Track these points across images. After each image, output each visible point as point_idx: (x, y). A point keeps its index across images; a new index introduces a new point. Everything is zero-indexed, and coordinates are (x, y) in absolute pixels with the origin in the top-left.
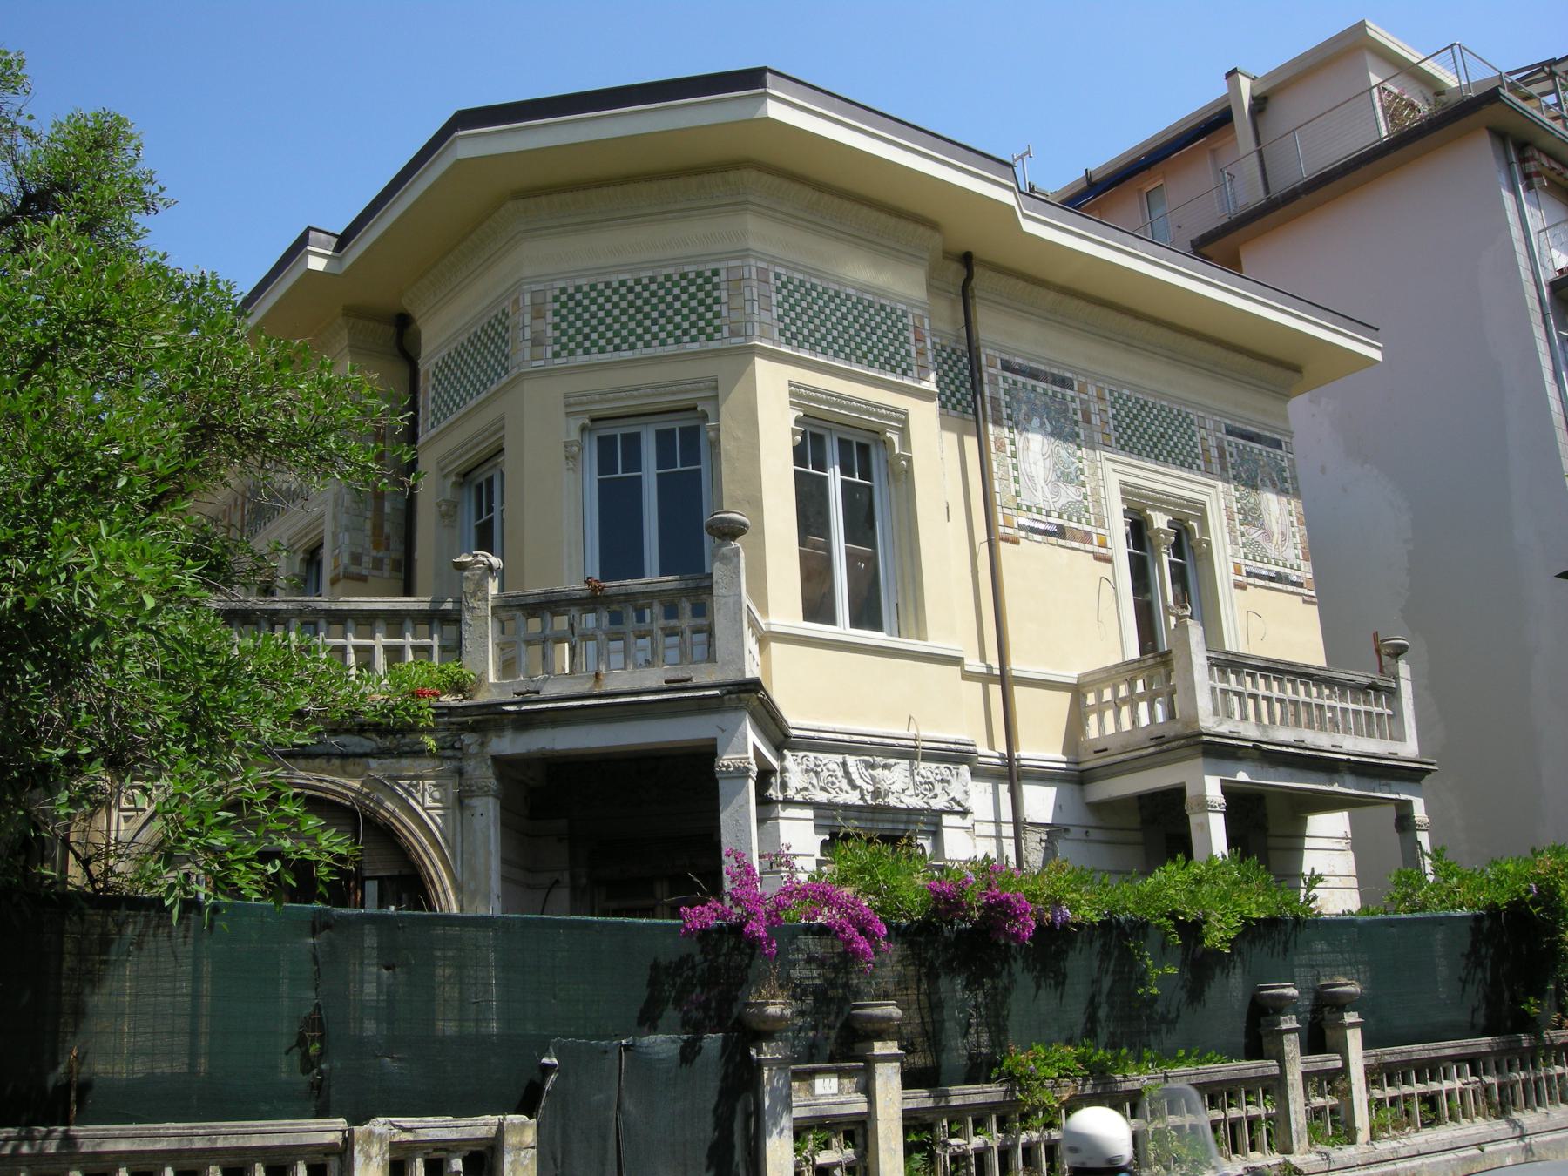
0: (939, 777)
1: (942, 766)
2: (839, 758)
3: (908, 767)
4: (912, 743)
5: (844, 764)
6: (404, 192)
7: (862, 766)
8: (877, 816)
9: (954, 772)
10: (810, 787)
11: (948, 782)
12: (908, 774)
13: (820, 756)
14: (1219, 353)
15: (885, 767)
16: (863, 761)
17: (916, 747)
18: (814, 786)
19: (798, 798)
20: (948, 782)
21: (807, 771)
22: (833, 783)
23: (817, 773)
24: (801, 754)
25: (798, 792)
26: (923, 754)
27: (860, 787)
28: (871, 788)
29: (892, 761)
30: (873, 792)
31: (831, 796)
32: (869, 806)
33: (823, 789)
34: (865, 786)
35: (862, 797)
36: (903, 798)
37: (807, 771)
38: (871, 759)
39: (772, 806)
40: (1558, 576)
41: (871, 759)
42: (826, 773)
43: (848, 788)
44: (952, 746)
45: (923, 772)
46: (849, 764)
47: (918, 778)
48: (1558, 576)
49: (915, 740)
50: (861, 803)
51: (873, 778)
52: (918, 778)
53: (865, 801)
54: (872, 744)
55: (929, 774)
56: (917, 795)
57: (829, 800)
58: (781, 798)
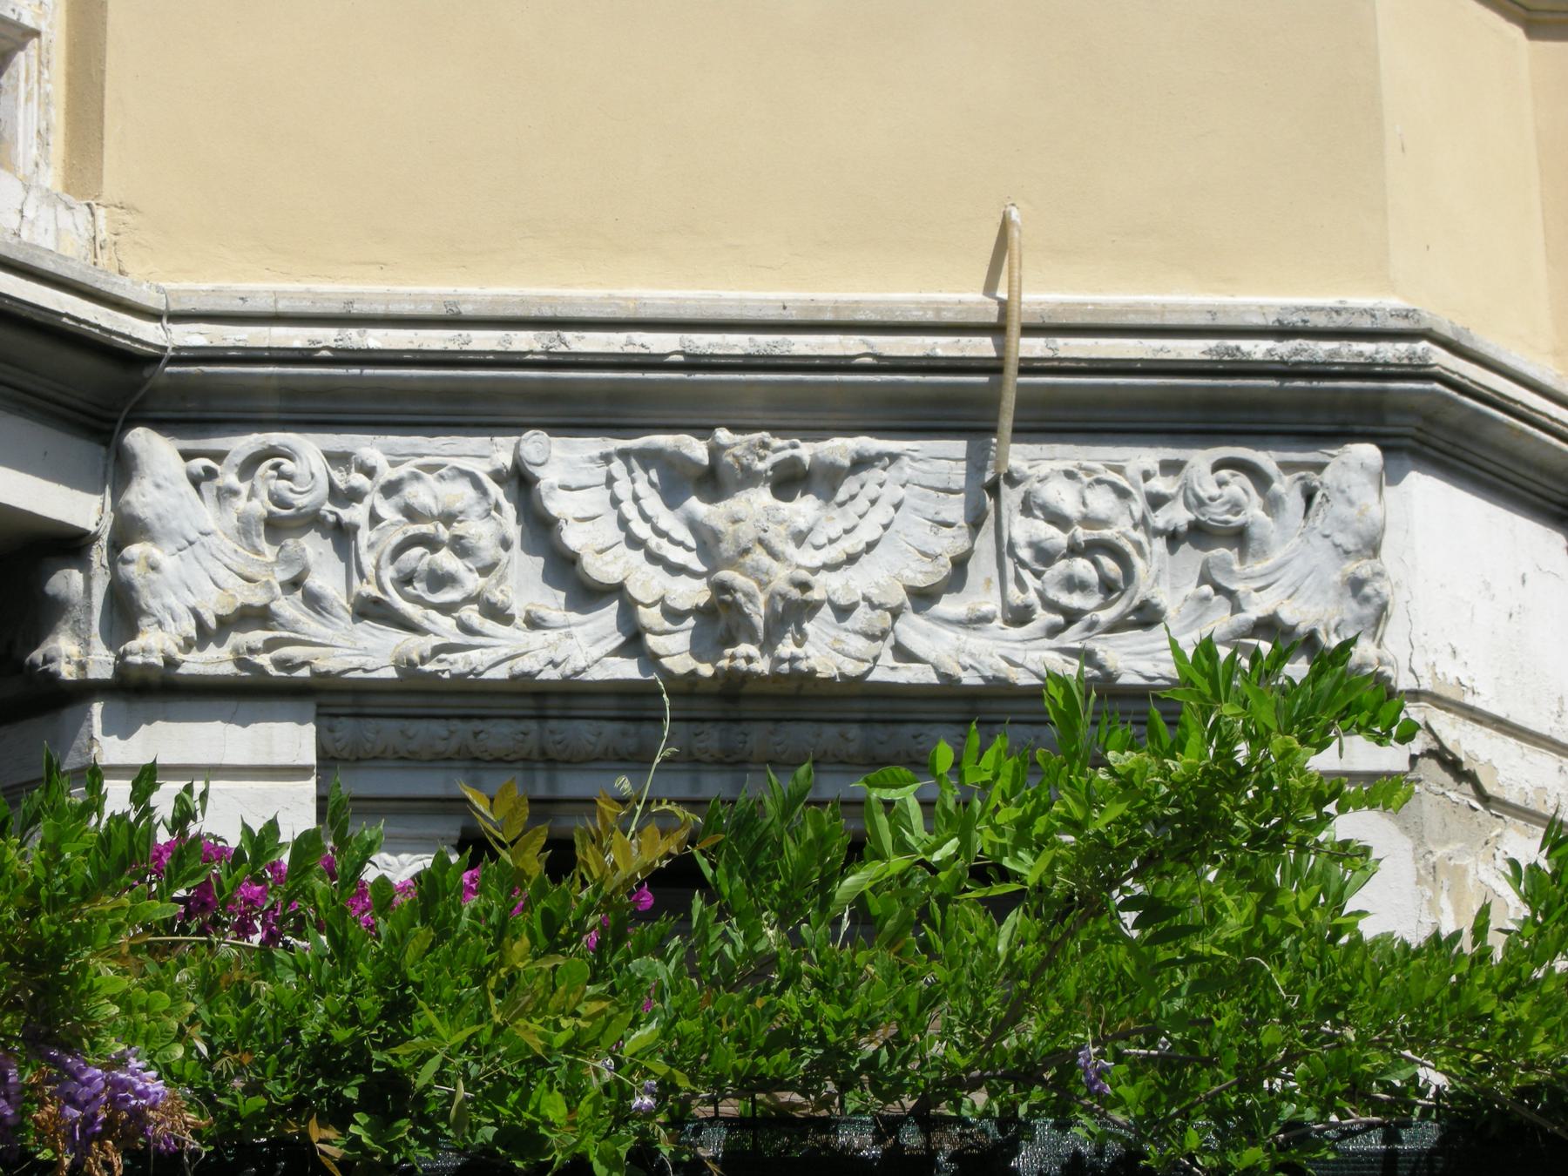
0: (1177, 516)
1: (1200, 459)
2: (500, 451)
3: (958, 474)
4: (982, 347)
5: (520, 481)
6: (138, 341)
7: (642, 486)
8: (757, 737)
9: (1285, 486)
10: (288, 607)
11: (1239, 537)
12: (955, 509)
13: (370, 447)
14: (439, 805)
15: (789, 481)
16: (648, 458)
17: (992, 368)
18: (314, 601)
19: (213, 662)
20: (1239, 537)
21: (276, 528)
22: (440, 580)
23: (342, 535)
24: (243, 444)
25: (205, 635)
26: (1026, 400)
27: (617, 591)
28: (691, 593)
29: (840, 448)
30: (706, 614)
31: (415, 645)
32: (687, 687)
33: (371, 610)
34: (646, 582)
35: (634, 642)
36: (914, 631)
37: (276, 528)
38: (697, 449)
39: (68, 714)
40: (245, 826)
41: (697, 449)
42: (396, 528)
43: (551, 602)
44: (1257, 349)
45: (1064, 497)
46: (548, 478)
47: (1023, 530)
48: (245, 826)
49: (996, 330)
50: (628, 669)
51: (706, 541)
52: (1023, 530)
53: (651, 660)
54: (694, 363)
55: (1102, 502)
56: (1019, 616)
57: (408, 668)
58: (101, 664)
